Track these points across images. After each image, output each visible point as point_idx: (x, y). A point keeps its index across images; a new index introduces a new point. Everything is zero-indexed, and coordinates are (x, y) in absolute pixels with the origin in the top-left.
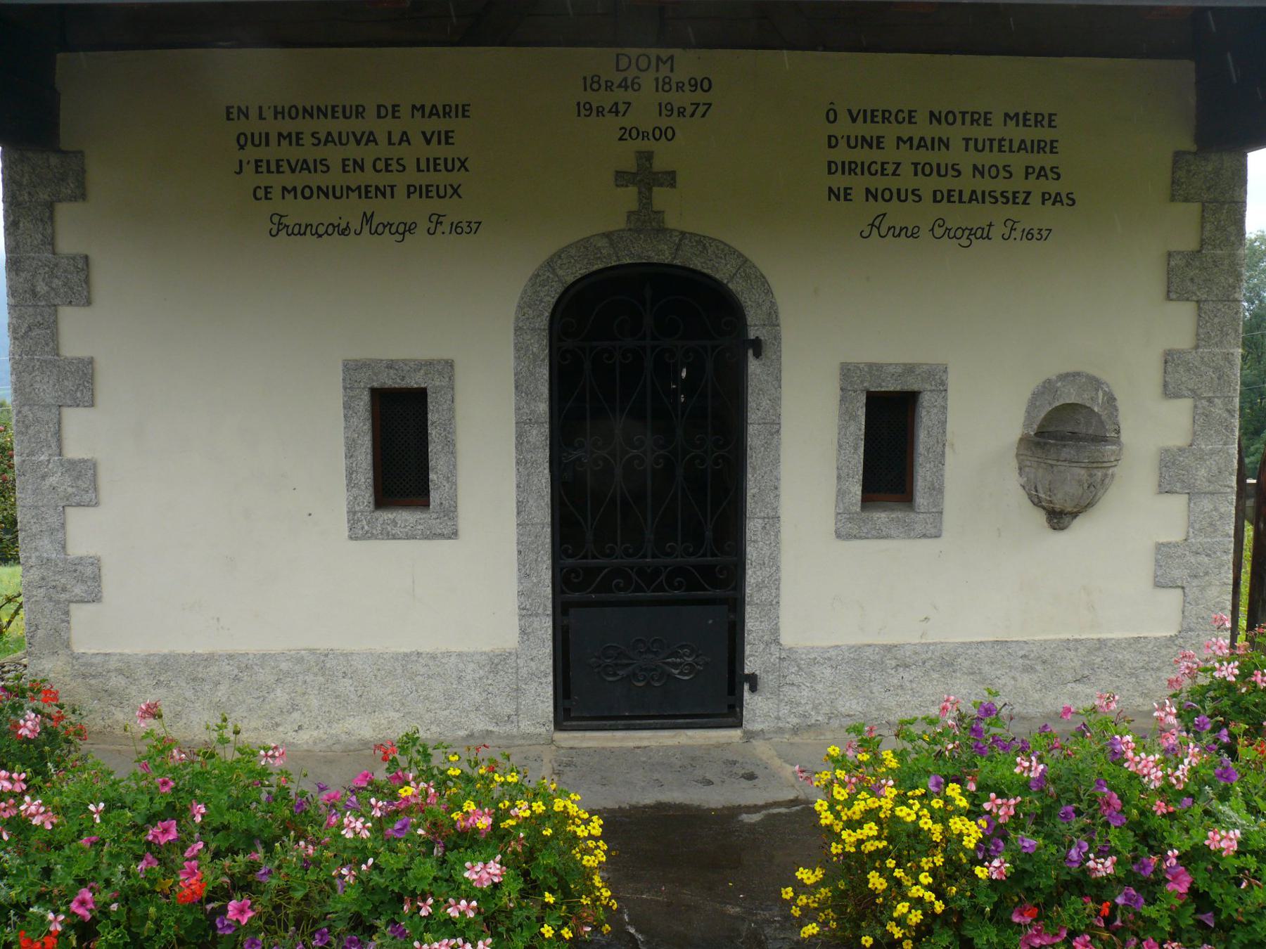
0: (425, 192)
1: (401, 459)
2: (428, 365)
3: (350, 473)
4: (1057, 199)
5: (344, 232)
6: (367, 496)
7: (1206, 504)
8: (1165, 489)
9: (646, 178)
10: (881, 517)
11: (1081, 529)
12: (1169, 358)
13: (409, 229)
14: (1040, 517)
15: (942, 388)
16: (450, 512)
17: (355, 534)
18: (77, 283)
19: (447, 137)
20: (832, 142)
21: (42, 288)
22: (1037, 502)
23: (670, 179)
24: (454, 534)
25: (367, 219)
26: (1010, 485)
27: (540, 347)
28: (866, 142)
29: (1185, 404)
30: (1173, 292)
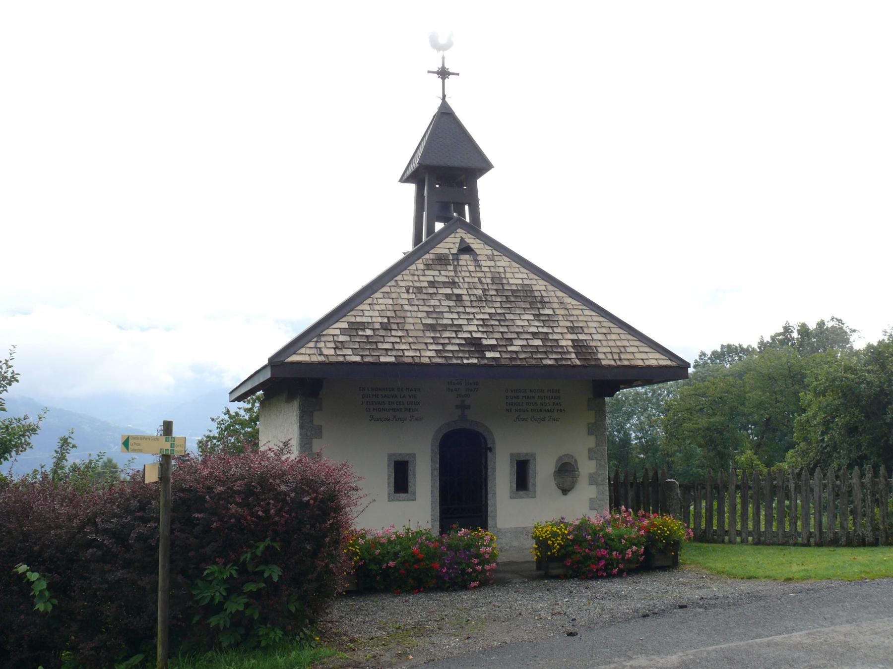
0: (409, 410)
1: (401, 482)
2: (410, 455)
3: (389, 483)
4: (561, 411)
5: (389, 420)
6: (393, 489)
7: (601, 487)
8: (591, 484)
9: (463, 407)
10: (521, 493)
11: (570, 495)
12: (590, 450)
13: (405, 420)
14: (560, 492)
15: (535, 459)
16: (414, 494)
17: (390, 500)
18: (318, 432)
19: (415, 397)
20: (507, 397)
21: (309, 434)
22: (559, 488)
23: (468, 407)
24: (415, 500)
25: (395, 417)
26: (553, 483)
27: (437, 450)
28: (515, 397)
29: (594, 462)
30: (590, 433)
